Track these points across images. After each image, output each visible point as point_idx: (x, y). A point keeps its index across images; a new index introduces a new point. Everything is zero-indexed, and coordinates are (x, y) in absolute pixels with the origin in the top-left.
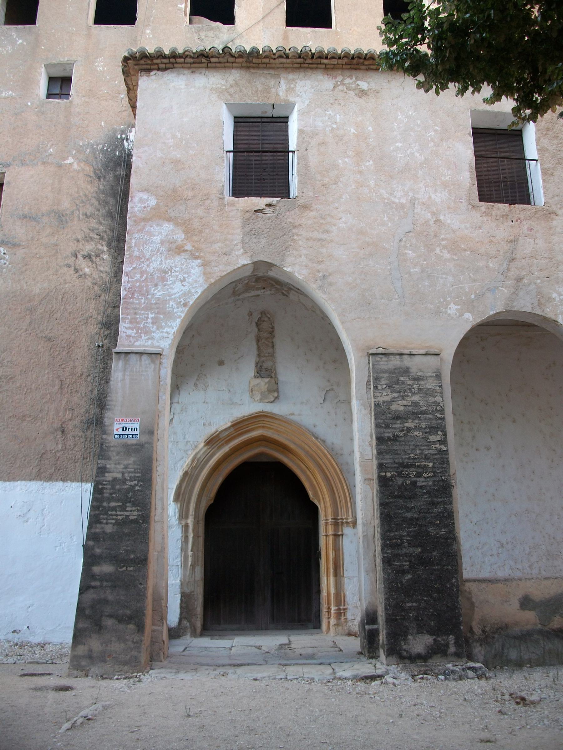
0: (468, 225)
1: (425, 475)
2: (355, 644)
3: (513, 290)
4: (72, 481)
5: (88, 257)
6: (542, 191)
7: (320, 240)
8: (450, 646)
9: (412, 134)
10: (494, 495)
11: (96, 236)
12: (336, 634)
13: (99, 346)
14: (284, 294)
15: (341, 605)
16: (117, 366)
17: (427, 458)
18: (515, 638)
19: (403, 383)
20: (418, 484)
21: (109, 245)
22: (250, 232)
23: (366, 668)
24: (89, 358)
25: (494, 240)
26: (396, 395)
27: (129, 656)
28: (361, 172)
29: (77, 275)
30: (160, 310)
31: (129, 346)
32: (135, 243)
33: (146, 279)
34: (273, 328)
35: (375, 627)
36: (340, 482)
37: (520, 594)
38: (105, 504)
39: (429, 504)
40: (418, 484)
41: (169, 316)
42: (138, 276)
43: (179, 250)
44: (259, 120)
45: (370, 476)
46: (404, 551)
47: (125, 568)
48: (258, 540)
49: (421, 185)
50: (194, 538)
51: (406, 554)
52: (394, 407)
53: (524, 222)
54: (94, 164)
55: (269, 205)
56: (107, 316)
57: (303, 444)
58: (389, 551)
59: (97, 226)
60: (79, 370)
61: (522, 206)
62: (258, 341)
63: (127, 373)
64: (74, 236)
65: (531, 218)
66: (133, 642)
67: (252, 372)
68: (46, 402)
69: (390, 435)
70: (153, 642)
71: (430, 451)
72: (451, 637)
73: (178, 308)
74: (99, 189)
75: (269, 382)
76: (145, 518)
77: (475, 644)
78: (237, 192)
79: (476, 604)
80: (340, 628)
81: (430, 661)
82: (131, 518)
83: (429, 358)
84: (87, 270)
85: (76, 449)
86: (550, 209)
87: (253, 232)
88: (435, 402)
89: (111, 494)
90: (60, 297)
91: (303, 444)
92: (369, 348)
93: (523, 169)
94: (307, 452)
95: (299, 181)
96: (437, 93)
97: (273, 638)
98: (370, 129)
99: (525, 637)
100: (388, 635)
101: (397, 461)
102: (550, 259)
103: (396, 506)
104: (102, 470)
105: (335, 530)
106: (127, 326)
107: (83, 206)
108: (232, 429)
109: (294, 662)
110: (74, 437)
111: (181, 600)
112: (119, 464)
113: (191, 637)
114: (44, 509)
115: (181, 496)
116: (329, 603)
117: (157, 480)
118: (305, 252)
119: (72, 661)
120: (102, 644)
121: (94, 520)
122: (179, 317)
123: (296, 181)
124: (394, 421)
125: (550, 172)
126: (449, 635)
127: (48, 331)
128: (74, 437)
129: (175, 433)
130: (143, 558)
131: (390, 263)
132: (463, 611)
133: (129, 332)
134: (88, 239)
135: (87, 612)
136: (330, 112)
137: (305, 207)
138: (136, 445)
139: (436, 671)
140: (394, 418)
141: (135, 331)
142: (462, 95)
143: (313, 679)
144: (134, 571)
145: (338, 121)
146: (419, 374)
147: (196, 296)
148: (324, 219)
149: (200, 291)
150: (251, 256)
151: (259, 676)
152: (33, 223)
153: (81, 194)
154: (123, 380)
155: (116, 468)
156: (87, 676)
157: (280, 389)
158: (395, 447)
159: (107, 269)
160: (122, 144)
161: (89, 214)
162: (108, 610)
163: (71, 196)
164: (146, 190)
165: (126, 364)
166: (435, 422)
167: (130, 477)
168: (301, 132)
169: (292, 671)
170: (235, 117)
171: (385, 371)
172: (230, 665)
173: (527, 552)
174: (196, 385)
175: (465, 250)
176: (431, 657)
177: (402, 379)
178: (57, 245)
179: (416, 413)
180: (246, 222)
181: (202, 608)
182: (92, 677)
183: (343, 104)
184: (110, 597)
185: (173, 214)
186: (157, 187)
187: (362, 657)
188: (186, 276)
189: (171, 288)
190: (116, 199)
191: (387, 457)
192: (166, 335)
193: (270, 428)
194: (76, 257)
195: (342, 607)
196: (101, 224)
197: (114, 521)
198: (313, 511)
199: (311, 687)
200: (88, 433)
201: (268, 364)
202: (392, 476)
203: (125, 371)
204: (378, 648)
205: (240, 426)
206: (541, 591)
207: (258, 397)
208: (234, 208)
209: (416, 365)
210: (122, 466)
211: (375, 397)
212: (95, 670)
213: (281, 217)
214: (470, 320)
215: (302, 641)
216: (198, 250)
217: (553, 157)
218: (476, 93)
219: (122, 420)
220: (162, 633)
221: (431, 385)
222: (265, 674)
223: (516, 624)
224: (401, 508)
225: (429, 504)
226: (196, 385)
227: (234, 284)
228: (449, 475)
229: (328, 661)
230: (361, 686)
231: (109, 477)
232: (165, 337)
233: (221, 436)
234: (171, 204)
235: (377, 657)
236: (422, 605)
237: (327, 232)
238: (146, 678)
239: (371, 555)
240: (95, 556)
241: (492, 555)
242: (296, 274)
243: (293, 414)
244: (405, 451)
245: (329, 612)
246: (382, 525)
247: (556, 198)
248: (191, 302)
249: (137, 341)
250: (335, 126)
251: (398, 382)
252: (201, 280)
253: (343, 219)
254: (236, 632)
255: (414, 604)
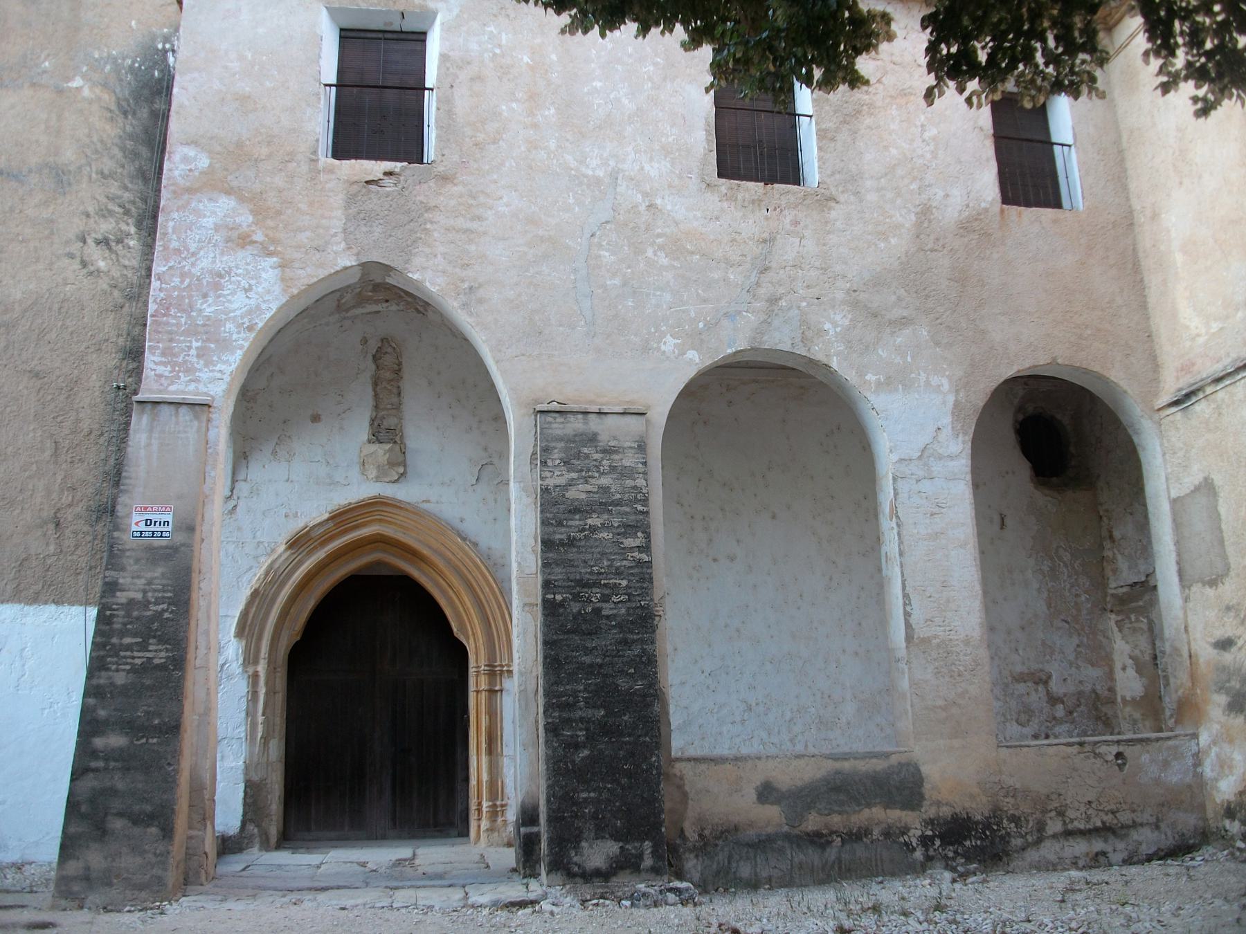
0: (699, 214)
1: (614, 599)
2: (509, 857)
3: (763, 317)
4: (72, 604)
5: (104, 242)
6: (816, 165)
7: (466, 231)
8: (645, 857)
9: (619, 67)
10: (738, 631)
11: (117, 209)
12: (488, 845)
13: (118, 387)
14: (418, 312)
15: (497, 799)
16: (140, 423)
17: (619, 573)
18: (749, 845)
19: (587, 456)
20: (604, 613)
21: (139, 224)
22: (358, 216)
23: (515, 891)
24: (102, 406)
25: (738, 238)
26: (575, 475)
27: (148, 877)
28: (535, 126)
29: (85, 271)
30: (211, 334)
31: (160, 392)
32: (174, 228)
33: (189, 285)
34: (400, 364)
35: (535, 829)
36: (500, 607)
37: (758, 779)
38: (115, 640)
39: (620, 643)
40: (604, 613)
41: (225, 345)
42: (177, 280)
43: (244, 241)
44: (380, 35)
45: (532, 600)
46: (579, 714)
47: (144, 740)
48: (370, 699)
49: (629, 149)
50: (267, 694)
51: (581, 719)
52: (571, 494)
53: (786, 212)
54: (118, 90)
55: (389, 174)
56: (133, 340)
57: (443, 548)
58: (556, 714)
59: (120, 193)
60: (85, 425)
61: (783, 186)
62: (375, 384)
63: (156, 435)
64: (81, 208)
65: (796, 206)
66: (155, 854)
67: (364, 434)
68: (30, 477)
69: (564, 537)
70: (189, 855)
71: (625, 563)
72: (647, 844)
73: (239, 333)
74: (124, 131)
75: (390, 450)
76: (178, 662)
77: (687, 855)
78: (339, 152)
79: (691, 796)
80: (496, 834)
81: (614, 879)
82: (157, 661)
83: (628, 419)
84: (102, 264)
85: (78, 552)
86: (827, 193)
87: (362, 216)
88: (635, 487)
89: (125, 624)
90: (56, 306)
91: (443, 548)
92: (537, 402)
93: (794, 127)
94: (449, 562)
95: (438, 137)
96: (603, 35)
97: (390, 850)
98: (554, 57)
99: (763, 844)
100: (551, 841)
101: (572, 577)
102: (824, 270)
103: (568, 646)
104: (111, 587)
105: (490, 684)
106: (157, 359)
107: (97, 160)
108: (331, 524)
109: (409, 883)
110: (76, 533)
111: (245, 792)
112: (138, 577)
113: (260, 850)
114: (23, 649)
115: (245, 628)
116: (479, 796)
117: (199, 604)
118: (441, 249)
119: (57, 885)
120: (106, 858)
121: (97, 665)
122: (241, 347)
123: (433, 136)
124: (571, 516)
125: (829, 135)
126: (643, 840)
127: (35, 362)
128: (76, 533)
129: (239, 529)
130: (173, 723)
131: (575, 271)
132: (667, 805)
133: (161, 369)
134: (104, 213)
135: (84, 808)
136: (492, 29)
137: (445, 179)
138: (167, 547)
139: (620, 894)
140: (570, 511)
141: (169, 368)
142: (644, 37)
143: (431, 907)
144: (158, 743)
145: (504, 42)
146: (612, 443)
147: (268, 315)
148: (474, 198)
149: (274, 307)
150: (358, 254)
151: (349, 903)
152: (14, 184)
153: (95, 139)
154: (149, 445)
155: (134, 584)
156: (81, 908)
157: (408, 463)
158: (570, 556)
159: (135, 263)
160: (165, 59)
161: (106, 172)
162: (116, 805)
163: (78, 141)
164: (194, 143)
165: (153, 420)
166: (633, 517)
167: (157, 598)
168: (444, 58)
169: (401, 897)
170: (342, 30)
171: (560, 439)
172: (310, 889)
173: (787, 718)
174: (274, 453)
175: (693, 253)
176: (615, 874)
177: (585, 450)
178: (52, 221)
179: (605, 504)
180: (351, 200)
181: (282, 807)
182: (90, 909)
183: (512, 16)
184: (120, 786)
185: (235, 183)
186: (212, 138)
187: (515, 876)
188: (253, 282)
189: (229, 301)
190: (153, 148)
191: (558, 570)
192: (219, 375)
193: (390, 523)
194: (85, 242)
195: (498, 803)
196: (126, 188)
197: (128, 667)
198: (459, 654)
199: (424, 918)
200: (99, 527)
201: (391, 422)
202: (564, 600)
203: (151, 431)
204: (538, 861)
205: (343, 518)
206: (790, 776)
207: (373, 473)
208: (333, 177)
209: (606, 429)
210: (143, 581)
211: (542, 478)
212: (94, 898)
213: (407, 193)
214: (695, 361)
215: (433, 854)
216: (274, 241)
217: (835, 112)
218: (667, 34)
219: (146, 508)
220: (203, 841)
221: (629, 460)
222: (360, 901)
223: (751, 825)
224: (577, 649)
225: (620, 643)
226: (274, 453)
227: (338, 294)
228: (652, 600)
229: (462, 882)
230: (502, 915)
231: (122, 597)
232: (218, 379)
233: (313, 534)
234: (232, 166)
235: (535, 875)
236: (604, 796)
237: (480, 218)
238: (173, 909)
239: (532, 719)
240: (97, 721)
241: (733, 723)
242: (428, 284)
243: (428, 501)
244: (585, 562)
245: (479, 810)
246: (546, 674)
247: (837, 176)
248: (260, 325)
249: (172, 383)
250: (498, 51)
251: (578, 456)
252: (277, 289)
253: (505, 200)
254: (334, 843)
255: (592, 795)
